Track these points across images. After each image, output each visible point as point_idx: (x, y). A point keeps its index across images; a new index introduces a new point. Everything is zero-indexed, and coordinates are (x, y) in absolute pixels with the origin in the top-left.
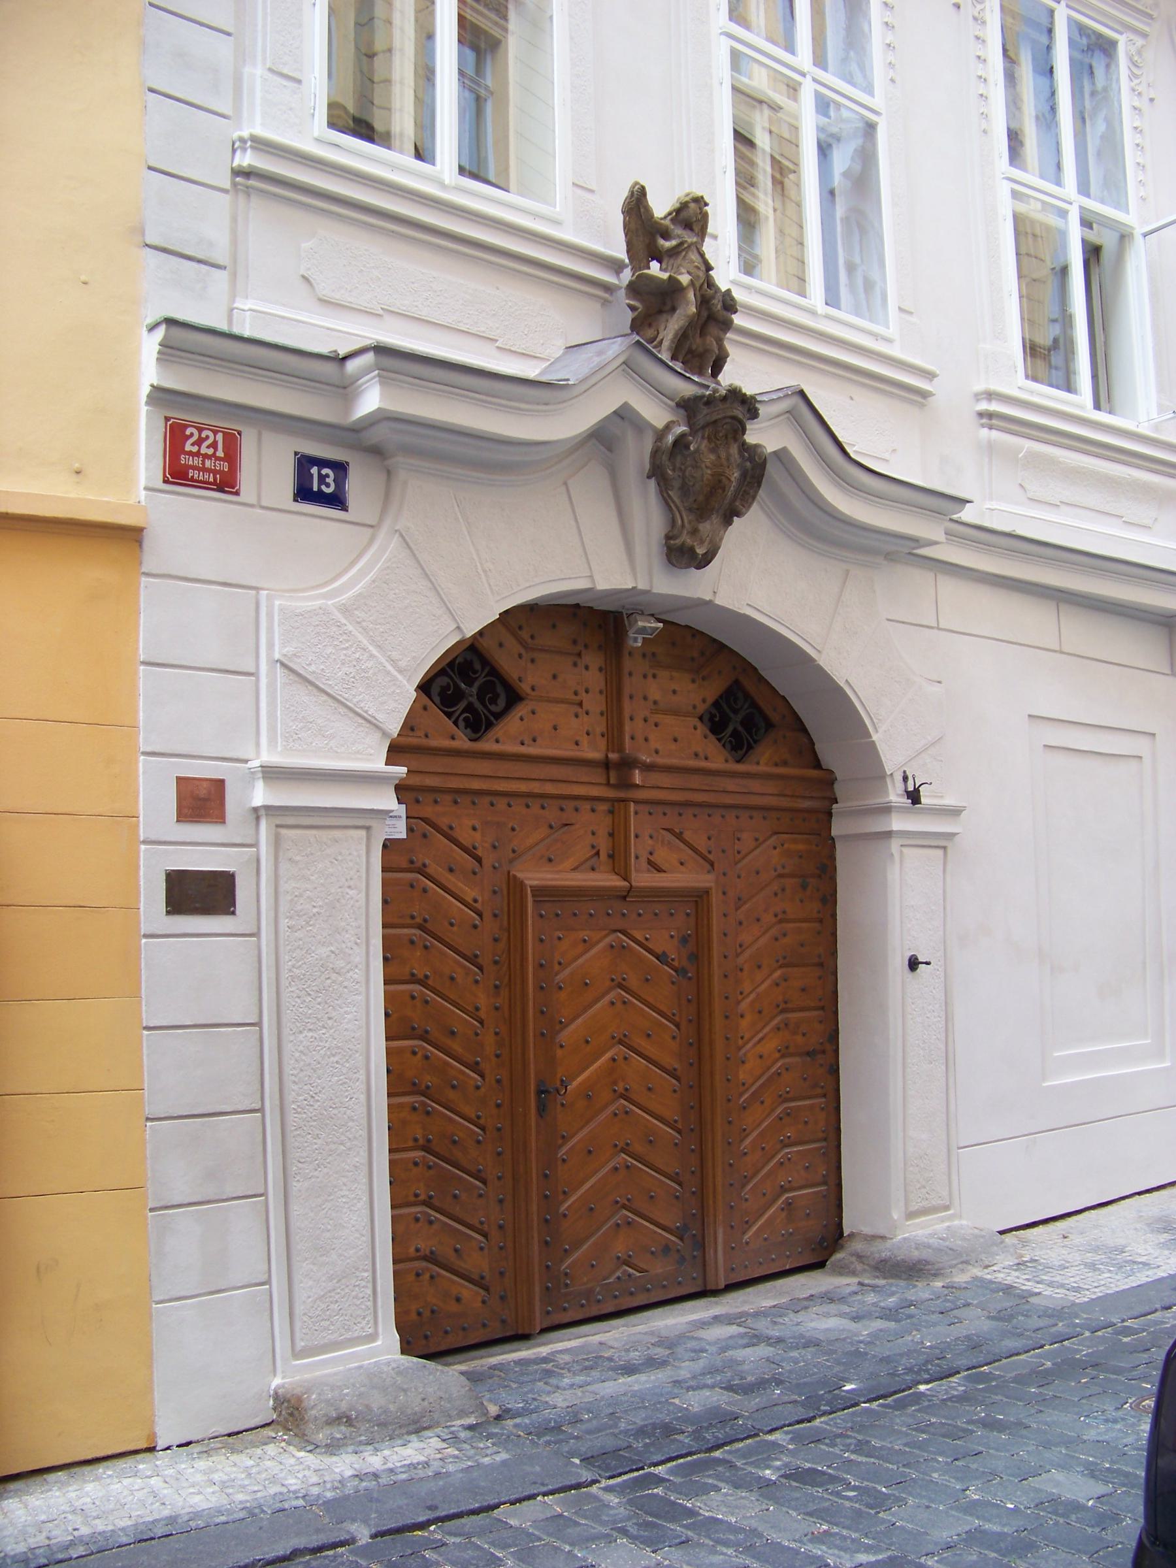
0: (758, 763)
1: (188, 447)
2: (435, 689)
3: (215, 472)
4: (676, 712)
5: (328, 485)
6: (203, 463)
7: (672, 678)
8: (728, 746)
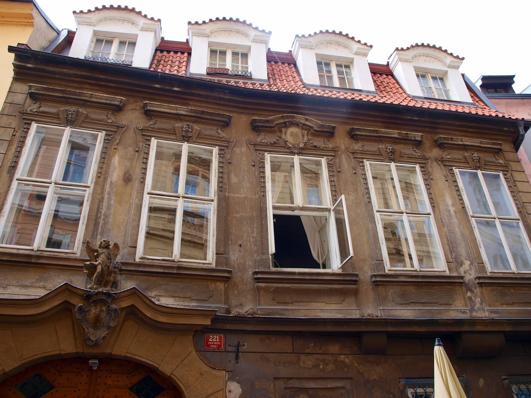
1: (210, 340)
3: (216, 345)
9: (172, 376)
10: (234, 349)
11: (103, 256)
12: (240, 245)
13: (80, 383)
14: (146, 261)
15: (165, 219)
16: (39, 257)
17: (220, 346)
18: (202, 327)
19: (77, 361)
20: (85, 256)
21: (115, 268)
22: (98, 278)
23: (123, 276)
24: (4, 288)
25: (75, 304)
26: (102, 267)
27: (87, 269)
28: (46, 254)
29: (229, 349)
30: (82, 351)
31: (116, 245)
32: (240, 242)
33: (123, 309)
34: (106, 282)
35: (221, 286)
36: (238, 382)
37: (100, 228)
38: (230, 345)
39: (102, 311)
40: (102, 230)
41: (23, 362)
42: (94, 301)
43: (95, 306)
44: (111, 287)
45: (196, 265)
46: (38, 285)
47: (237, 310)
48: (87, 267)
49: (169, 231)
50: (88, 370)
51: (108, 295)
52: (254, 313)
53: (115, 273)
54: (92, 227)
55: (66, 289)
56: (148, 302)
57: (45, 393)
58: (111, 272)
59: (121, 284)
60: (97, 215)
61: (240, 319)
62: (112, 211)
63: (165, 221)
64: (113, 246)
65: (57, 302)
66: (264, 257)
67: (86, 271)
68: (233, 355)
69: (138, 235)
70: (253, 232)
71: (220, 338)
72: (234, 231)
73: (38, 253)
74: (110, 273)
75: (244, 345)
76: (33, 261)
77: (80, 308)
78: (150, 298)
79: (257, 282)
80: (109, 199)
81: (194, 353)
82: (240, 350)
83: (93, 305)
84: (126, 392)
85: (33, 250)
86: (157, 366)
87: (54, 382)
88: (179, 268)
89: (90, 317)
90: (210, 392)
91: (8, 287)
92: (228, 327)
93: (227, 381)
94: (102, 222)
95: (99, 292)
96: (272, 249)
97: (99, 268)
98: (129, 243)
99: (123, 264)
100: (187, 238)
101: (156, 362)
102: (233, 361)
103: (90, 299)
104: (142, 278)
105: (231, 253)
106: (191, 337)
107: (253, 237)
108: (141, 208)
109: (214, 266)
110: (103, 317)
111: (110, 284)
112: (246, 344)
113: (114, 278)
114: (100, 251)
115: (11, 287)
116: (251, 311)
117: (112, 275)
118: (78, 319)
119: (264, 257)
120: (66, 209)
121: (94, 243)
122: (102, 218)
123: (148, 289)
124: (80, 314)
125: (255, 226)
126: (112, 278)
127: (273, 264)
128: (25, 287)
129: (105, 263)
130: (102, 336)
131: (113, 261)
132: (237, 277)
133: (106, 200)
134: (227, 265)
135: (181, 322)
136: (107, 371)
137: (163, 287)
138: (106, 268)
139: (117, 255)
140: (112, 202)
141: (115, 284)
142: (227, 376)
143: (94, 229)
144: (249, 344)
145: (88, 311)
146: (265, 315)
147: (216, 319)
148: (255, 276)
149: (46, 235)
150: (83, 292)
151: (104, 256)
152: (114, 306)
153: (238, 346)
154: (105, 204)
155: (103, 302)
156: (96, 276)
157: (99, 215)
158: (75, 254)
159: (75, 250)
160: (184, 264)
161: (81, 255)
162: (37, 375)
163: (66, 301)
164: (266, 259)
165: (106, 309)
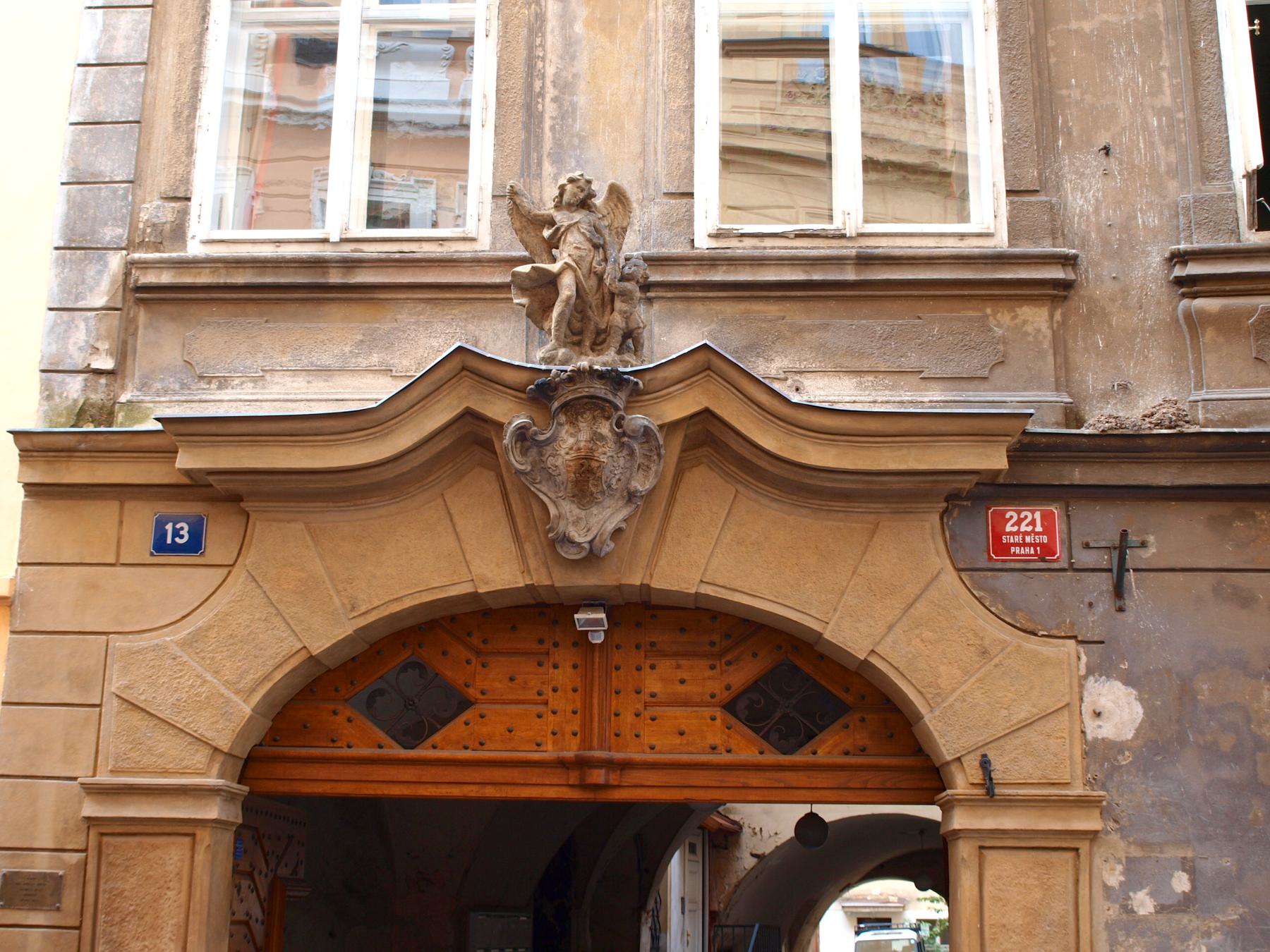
0: (815, 753)
1: (1008, 528)
2: (741, 705)
3: (1035, 545)
4: (685, 703)
5: (182, 537)
6: (1024, 539)
7: (678, 667)
8: (774, 736)
9: (874, 660)
10: (1103, 559)
11: (573, 238)
12: (1107, 150)
13: (555, 690)
14: (734, 243)
17: (1047, 550)
18: (975, 479)
22: (569, 324)
23: (656, 306)
24: (255, 380)
25: (502, 420)
26: (576, 277)
27: (523, 290)
29: (1086, 558)
30: (548, 583)
31: (616, 194)
32: (1103, 139)
34: (599, 332)
35: (1036, 318)
36: (1128, 680)
37: (548, 134)
38: (1087, 546)
39: (597, 437)
40: (558, 143)
41: (362, 622)
42: (565, 407)
43: (573, 423)
44: (619, 352)
45: (931, 242)
46: (364, 363)
47: (1109, 410)
49: (806, 134)
50: (575, 644)
51: (614, 379)
52: (1181, 418)
53: (626, 296)
54: (517, 135)
55: (463, 369)
56: (764, 398)
58: (613, 295)
60: (530, 86)
61: (1123, 445)
62: (582, 64)
64: (608, 199)
65: (439, 415)
66: (1213, 189)
67: (524, 301)
68: (1104, 582)
69: (691, 148)
70: (1156, 91)
71: (1047, 517)
72: (1075, 94)
73: (347, 250)
75: (1144, 545)
76: (335, 278)
77: (522, 435)
78: (767, 382)
79: (1184, 295)
80: (566, 20)
81: (950, 576)
82: (1130, 563)
83: (562, 418)
84: (713, 719)
85: (325, 241)
86: (816, 626)
88: (865, 260)
89: (559, 462)
90: (1023, 715)
91: (268, 377)
92: (1077, 475)
93: (1086, 677)
95: (579, 373)
96: (1246, 150)
97: (567, 287)
100: (881, 155)
101: (813, 612)
102: (1105, 605)
103: (551, 399)
105: (1068, 186)
106: (936, 518)
107: (1159, 112)
108: (692, 37)
109: (1001, 242)
110: (604, 459)
111: (615, 340)
112: (1151, 539)
113: (627, 316)
114: (562, 218)
115: (277, 378)
116: (1169, 411)
117: (618, 305)
118: (519, 472)
119: (1213, 189)
120: (419, 89)
121: (536, 195)
122: (548, 97)
123: (754, 348)
124: (524, 452)
125: (1165, 61)
126: (617, 319)
127: (1251, 214)
128: (324, 372)
129: (585, 265)
130: (610, 527)
131: (612, 252)
132: (1099, 279)
133: (552, 24)
134: (1055, 234)
135: (892, 466)
137: (807, 336)
138: (593, 282)
139: (624, 230)
140: (578, 28)
141: (631, 339)
142: (1084, 658)
143: (527, 141)
144: (1166, 537)
145: (548, 442)
146: (1223, 423)
147: (1029, 449)
148: (1179, 271)
151: (580, 238)
152: (638, 419)
153: (1122, 547)
154: (553, 39)
155: (597, 406)
156: (561, 314)
158: (473, 240)
159: (470, 228)
160: (883, 242)
161: (493, 243)
163: (469, 414)
164: (1221, 197)
165: (612, 430)
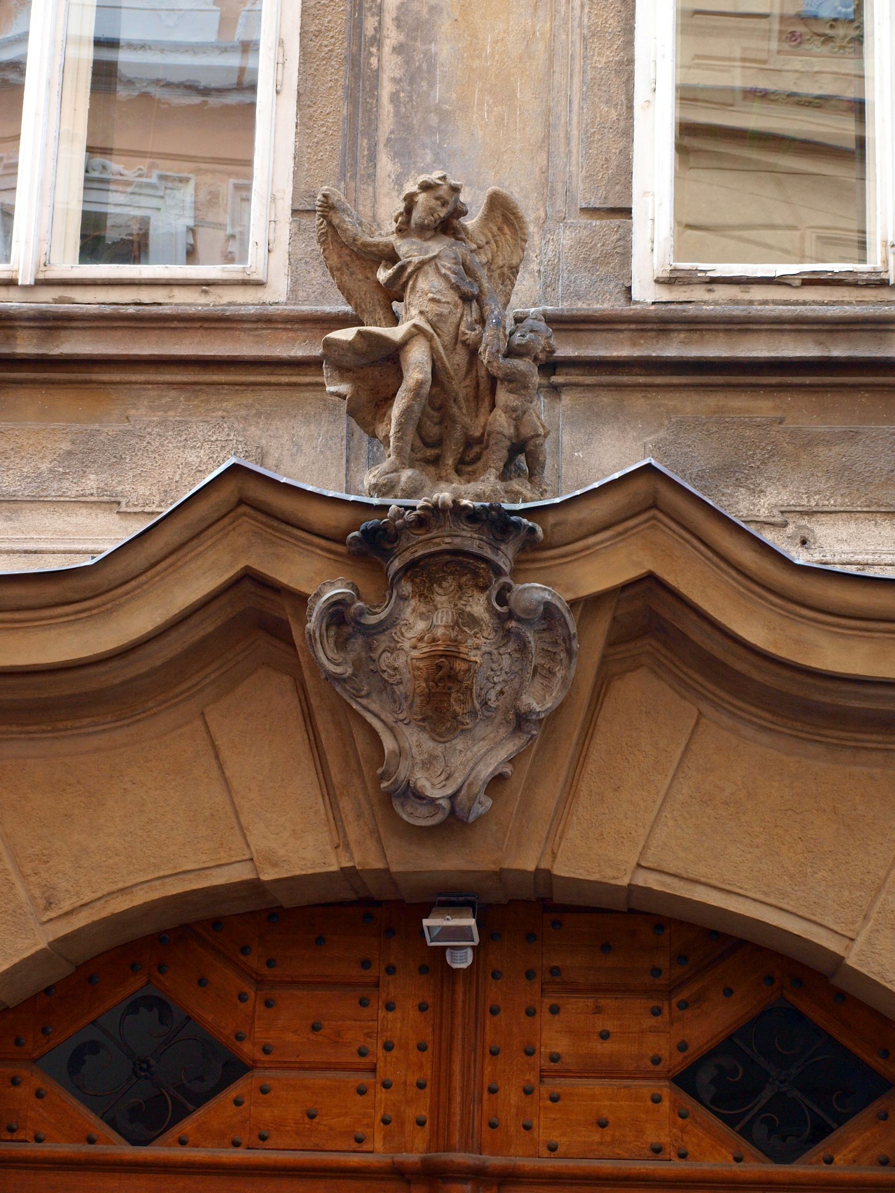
0: (829, 1161)
4: (608, 1071)
7: (598, 1010)
13: (388, 1047)
14: (698, 293)
15: (762, 24)
16: (52, 323)
19: (347, 926)
20: (323, 296)
21: (512, 352)
22: (419, 428)
23: (566, 400)
25: (304, 588)
26: (433, 350)
27: (343, 371)
28: (88, 301)
30: (380, 865)
31: (501, 209)
33: (588, 605)
34: (469, 442)
37: (387, 107)
40: (403, 123)
42: (411, 568)
43: (425, 596)
44: (504, 476)
46: (72, 490)
48: (341, 361)
51: (494, 522)
53: (516, 382)
54: (334, 108)
55: (241, 502)
56: (747, 557)
57: (200, 1100)
58: (493, 381)
59: (557, 451)
60: (357, 26)
63: (766, 35)
65: (198, 581)
67: (344, 388)
69: (627, 133)
73: (45, 300)
74: (487, 387)
77: (338, 614)
78: (752, 529)
83: (407, 588)
84: (657, 1100)
86: (833, 944)
87: (239, 1038)
89: (401, 661)
94: (390, 66)
95: (435, 511)
97: (417, 365)
98: (580, 186)
99: (564, 324)
101: (828, 921)
103: (388, 555)
104: (692, 405)
110: (475, 657)
111: (497, 456)
113: (517, 416)
114: (410, 250)
117: (503, 396)
121: (365, 210)
122: (388, 45)
123: (730, 472)
124: (342, 644)
126: (501, 421)
129: (448, 329)
130: (486, 771)
131: (493, 308)
136: (530, 975)
137: (822, 452)
138: (461, 357)
141: (524, 454)
143: (351, 119)
145: (382, 627)
149: (72, 202)
150: (342, 517)
152: (534, 591)
155: (466, 568)
157: (370, 23)
158: (259, 284)
159: (255, 263)
161: (293, 291)
162: (152, 1001)
163: (249, 580)
165: (490, 609)
